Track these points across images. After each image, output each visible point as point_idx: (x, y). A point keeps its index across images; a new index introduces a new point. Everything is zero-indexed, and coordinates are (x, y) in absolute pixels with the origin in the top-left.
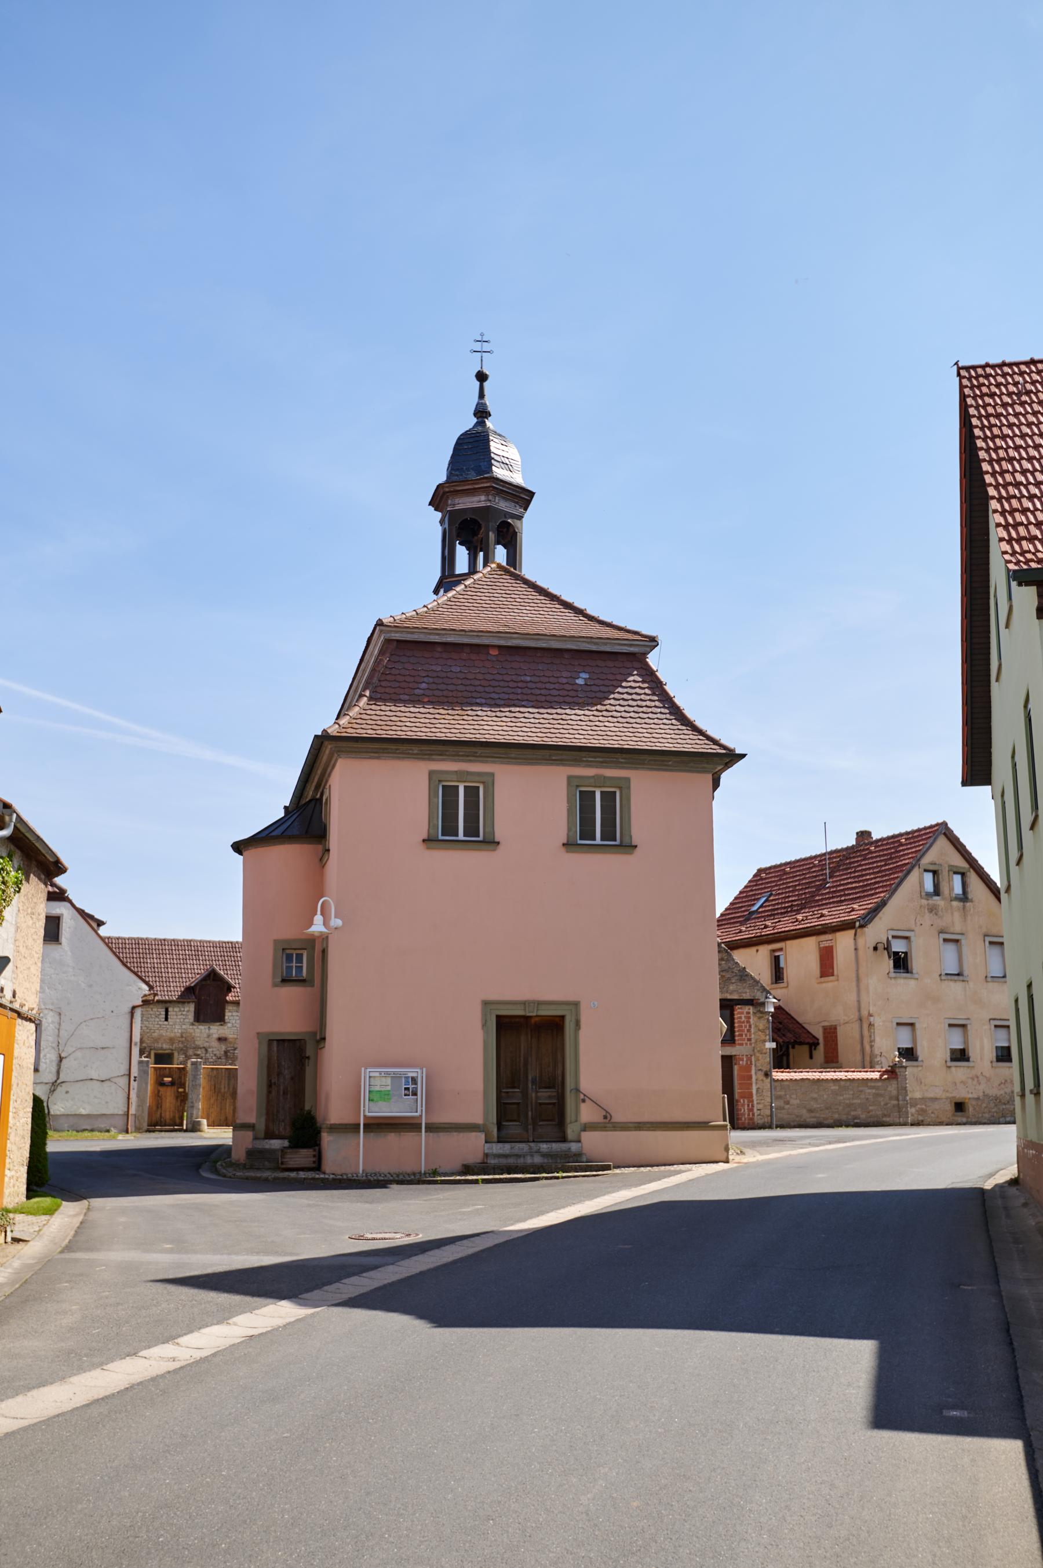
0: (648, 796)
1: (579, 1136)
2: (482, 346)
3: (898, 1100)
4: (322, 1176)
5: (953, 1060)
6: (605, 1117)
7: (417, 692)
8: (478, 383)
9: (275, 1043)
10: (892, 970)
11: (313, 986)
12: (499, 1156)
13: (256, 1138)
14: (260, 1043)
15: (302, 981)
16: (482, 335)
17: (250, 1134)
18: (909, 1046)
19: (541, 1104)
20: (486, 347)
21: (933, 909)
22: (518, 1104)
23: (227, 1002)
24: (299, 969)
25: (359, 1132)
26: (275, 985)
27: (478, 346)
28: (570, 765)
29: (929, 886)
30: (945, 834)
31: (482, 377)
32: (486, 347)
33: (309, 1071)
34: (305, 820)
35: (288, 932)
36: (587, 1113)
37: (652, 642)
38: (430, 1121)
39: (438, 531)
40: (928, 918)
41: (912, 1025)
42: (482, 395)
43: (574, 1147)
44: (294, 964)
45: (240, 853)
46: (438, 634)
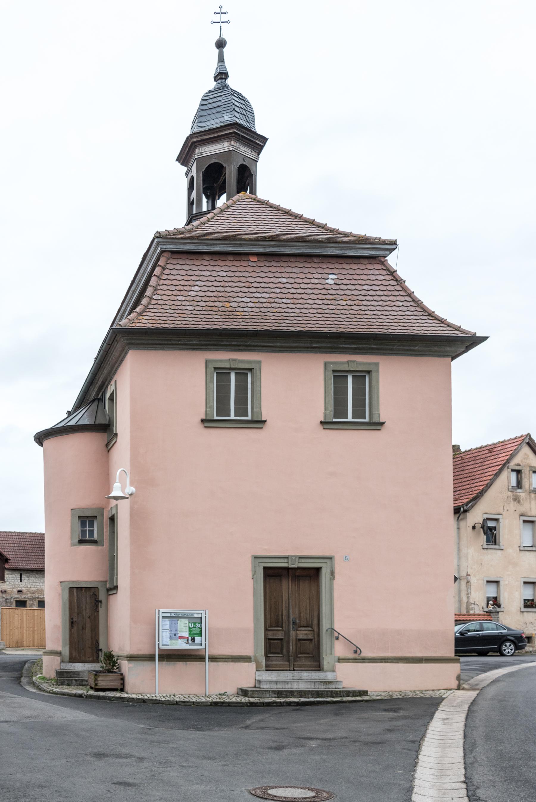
1: (334, 666)
2: (221, 17)
5: (526, 606)
6: (355, 652)
7: (192, 293)
8: (217, 51)
9: (75, 589)
10: (485, 543)
12: (271, 682)
14: (63, 590)
15: (95, 542)
16: (221, 7)
17: (58, 659)
18: (495, 596)
19: (300, 640)
20: (224, 18)
21: (516, 499)
23: (6, 569)
24: (91, 533)
25: (155, 661)
26: (73, 545)
27: (217, 18)
28: (326, 352)
29: (514, 483)
30: (528, 444)
31: (221, 44)
32: (224, 18)
33: (101, 611)
35: (86, 501)
36: (340, 649)
37: (391, 245)
38: (210, 654)
40: (513, 506)
41: (497, 582)
42: (221, 59)
43: (330, 676)
44: (87, 529)
45: (41, 444)
46: (206, 244)
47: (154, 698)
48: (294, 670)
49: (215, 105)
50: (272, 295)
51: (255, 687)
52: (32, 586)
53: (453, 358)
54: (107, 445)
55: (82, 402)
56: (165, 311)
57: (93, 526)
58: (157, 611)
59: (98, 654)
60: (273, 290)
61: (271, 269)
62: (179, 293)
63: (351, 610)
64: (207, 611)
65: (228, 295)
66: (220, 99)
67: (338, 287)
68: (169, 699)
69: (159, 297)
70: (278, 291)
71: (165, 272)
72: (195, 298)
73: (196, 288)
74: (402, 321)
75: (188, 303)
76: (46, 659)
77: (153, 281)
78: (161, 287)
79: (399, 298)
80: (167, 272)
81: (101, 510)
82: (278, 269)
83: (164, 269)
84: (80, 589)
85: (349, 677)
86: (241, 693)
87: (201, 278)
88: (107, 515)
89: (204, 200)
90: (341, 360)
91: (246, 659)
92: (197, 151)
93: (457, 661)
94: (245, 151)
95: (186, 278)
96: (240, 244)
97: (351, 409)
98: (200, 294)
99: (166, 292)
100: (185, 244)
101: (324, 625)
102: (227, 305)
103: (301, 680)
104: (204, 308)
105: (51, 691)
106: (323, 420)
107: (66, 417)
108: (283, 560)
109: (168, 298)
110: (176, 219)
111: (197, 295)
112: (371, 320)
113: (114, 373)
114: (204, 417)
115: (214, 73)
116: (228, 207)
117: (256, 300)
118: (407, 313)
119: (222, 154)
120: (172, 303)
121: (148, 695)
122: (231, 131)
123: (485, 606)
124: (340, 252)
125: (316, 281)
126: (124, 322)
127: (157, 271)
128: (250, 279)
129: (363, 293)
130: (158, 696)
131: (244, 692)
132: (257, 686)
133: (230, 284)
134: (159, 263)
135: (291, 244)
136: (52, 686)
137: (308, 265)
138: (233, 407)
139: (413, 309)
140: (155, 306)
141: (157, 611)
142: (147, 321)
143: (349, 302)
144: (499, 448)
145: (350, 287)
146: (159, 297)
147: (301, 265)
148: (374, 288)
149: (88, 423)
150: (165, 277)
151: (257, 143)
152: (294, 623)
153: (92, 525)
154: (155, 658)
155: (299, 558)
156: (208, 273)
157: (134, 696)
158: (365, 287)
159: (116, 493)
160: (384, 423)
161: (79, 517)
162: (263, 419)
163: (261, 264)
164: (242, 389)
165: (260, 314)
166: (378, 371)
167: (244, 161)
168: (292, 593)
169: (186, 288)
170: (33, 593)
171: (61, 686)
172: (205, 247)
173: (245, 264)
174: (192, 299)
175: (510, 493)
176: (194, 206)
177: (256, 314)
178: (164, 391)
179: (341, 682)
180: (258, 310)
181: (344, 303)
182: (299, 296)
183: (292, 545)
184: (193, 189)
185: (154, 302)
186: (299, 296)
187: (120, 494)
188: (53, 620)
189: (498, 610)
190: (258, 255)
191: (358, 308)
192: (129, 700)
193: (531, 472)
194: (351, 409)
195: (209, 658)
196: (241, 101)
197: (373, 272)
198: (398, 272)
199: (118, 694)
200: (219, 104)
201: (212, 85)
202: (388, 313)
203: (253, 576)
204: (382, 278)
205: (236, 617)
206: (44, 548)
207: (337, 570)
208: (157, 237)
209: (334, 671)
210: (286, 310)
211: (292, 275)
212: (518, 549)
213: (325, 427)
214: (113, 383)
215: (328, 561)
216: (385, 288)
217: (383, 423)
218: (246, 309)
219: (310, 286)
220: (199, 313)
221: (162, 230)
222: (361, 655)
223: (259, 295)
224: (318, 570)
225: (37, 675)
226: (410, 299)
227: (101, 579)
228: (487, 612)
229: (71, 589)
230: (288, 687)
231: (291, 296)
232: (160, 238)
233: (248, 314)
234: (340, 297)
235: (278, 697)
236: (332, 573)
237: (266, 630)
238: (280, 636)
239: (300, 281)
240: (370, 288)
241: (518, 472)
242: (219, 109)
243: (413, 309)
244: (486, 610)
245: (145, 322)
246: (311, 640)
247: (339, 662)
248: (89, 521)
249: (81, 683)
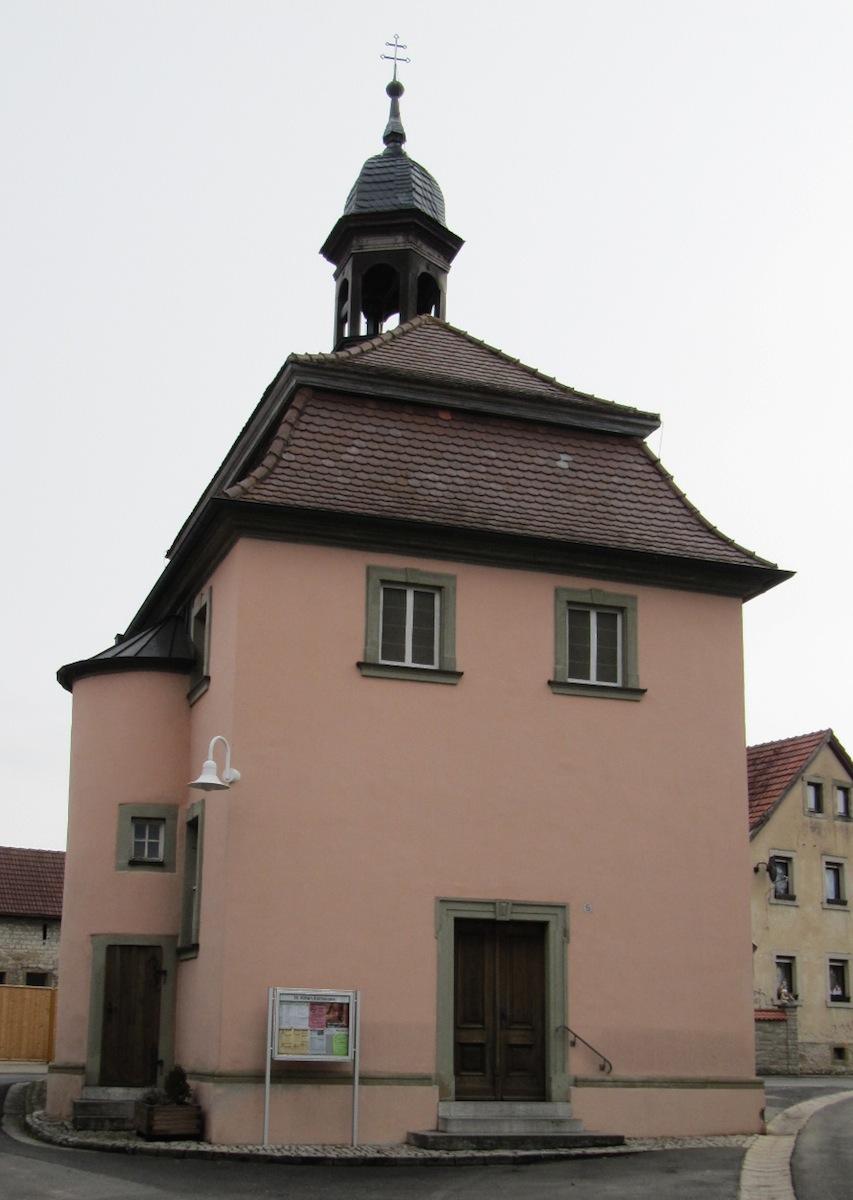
0: (659, 622)
3: (787, 1044)
4: (209, 1148)
6: (602, 1068)
7: (345, 457)
8: (389, 99)
11: (174, 871)
13: (87, 1085)
14: (95, 949)
15: (159, 865)
16: (397, 37)
17: (79, 1079)
20: (401, 53)
21: (815, 828)
22: (481, 1045)
24: (154, 848)
25: (264, 1082)
26: (119, 868)
27: (390, 51)
29: (811, 804)
31: (395, 90)
32: (401, 53)
33: (165, 989)
34: (169, 634)
35: (148, 791)
36: (578, 1063)
37: (651, 421)
39: (331, 289)
42: (395, 112)
44: (146, 840)
46: (372, 384)
47: (262, 1152)
48: (502, 1100)
49: (385, 178)
50: (474, 475)
51: (437, 1130)
52: (17, 947)
53: (744, 601)
54: (189, 696)
55: (146, 619)
56: (302, 480)
57: (160, 834)
58: (271, 990)
59: (156, 1070)
60: (476, 468)
61: (472, 435)
62: (325, 455)
63: (594, 995)
64: (359, 993)
65: (404, 466)
66: (392, 170)
67: (573, 474)
68: (289, 1154)
69: (293, 457)
70: (483, 469)
71: (302, 418)
72: (351, 466)
73: (354, 450)
74: (670, 535)
75: (340, 472)
76: (54, 1081)
77: (283, 430)
78: (297, 442)
79: (664, 501)
80: (305, 418)
81: (173, 809)
82: (484, 436)
83: (301, 413)
84: (127, 949)
85: (589, 1111)
86: (413, 1141)
87: (361, 435)
88: (183, 819)
89: (363, 321)
90: (581, 586)
91: (423, 1080)
92: (354, 242)
93: (759, 1085)
94: (428, 253)
95: (337, 432)
96: (424, 391)
97: (595, 664)
98: (359, 459)
99: (304, 451)
100: (336, 378)
101: (552, 1021)
102: (402, 481)
103: (511, 1118)
104: (366, 483)
105: (65, 1142)
106: (552, 679)
107: (113, 644)
108: (486, 908)
109: (306, 460)
110: (319, 341)
111: (344, 463)
112: (624, 530)
113: (209, 575)
114: (362, 660)
115: (384, 131)
116: (404, 333)
117: (449, 480)
118: (676, 524)
119: (391, 243)
120: (313, 468)
121: (250, 1147)
122: (410, 220)
123: (775, 997)
124: (577, 423)
125: (542, 462)
126: (232, 492)
127: (291, 415)
128: (440, 447)
129: (612, 487)
130: (268, 1146)
131: (420, 1141)
132: (440, 1128)
133: (409, 450)
134: (293, 404)
135: (505, 400)
136: (65, 1131)
137: (529, 436)
138: (408, 645)
139: (686, 520)
140: (286, 471)
141: (271, 990)
142: (271, 493)
143: (591, 499)
144: (788, 749)
145: (592, 476)
146: (293, 457)
147: (519, 434)
148: (627, 481)
149: (158, 655)
150: (303, 426)
151: (449, 245)
152: (503, 1016)
153: (155, 834)
154: (264, 1077)
155: (514, 904)
156: (374, 429)
157: (224, 1149)
158: (616, 479)
159: (208, 777)
160: (645, 691)
161: (133, 818)
162: (458, 669)
163: (456, 425)
164: (424, 619)
165: (455, 501)
166: (635, 609)
167: (428, 268)
168: (501, 965)
169: (336, 448)
170: (19, 959)
171: (84, 1132)
172: (370, 388)
173: (432, 421)
174: (345, 465)
175: (807, 819)
176: (347, 326)
177: (448, 501)
178: (291, 611)
179: (580, 1120)
180: (452, 495)
181: (585, 499)
182: (516, 481)
183: (504, 882)
184: (347, 299)
185: (282, 464)
186: (516, 481)
187: (215, 780)
188: (75, 1001)
189: (796, 1003)
190: (454, 411)
191: (604, 509)
192: (215, 1156)
193: (835, 788)
194: (595, 664)
195: (360, 1078)
196: (424, 179)
197: (627, 459)
198: (661, 462)
199: (193, 1146)
200: (392, 177)
201: (380, 148)
202: (649, 522)
203: (437, 933)
204: (640, 468)
205: (410, 1004)
206: (63, 869)
207: (573, 927)
208: (292, 362)
209: (568, 1101)
210: (496, 500)
211: (504, 448)
212: (820, 906)
213: (556, 690)
214: (205, 590)
215: (558, 911)
216: (643, 484)
217: (644, 691)
218: (433, 492)
219: (532, 467)
220: (357, 489)
221: (301, 351)
222: (612, 1073)
223: (454, 473)
224: (542, 927)
225: (33, 1110)
226: (681, 505)
227: (169, 932)
228: (779, 1007)
229: (111, 949)
230: (492, 1131)
231: (504, 480)
232: (296, 365)
233: (436, 499)
234: (577, 490)
235: (479, 1149)
236: (566, 933)
237: (457, 1028)
238: (477, 1038)
239: (518, 458)
240: (622, 480)
241: (818, 787)
242: (391, 186)
243: (686, 520)
244: (778, 1002)
245: (268, 495)
246: (530, 1047)
247: (576, 1086)
248: (151, 827)
249: (118, 1125)
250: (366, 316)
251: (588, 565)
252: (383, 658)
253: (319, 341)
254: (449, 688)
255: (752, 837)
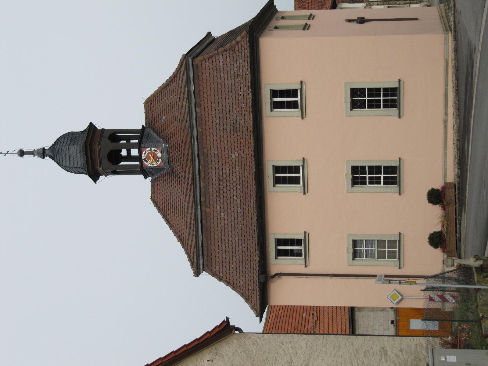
8: (25, 156)
31: (22, 153)
42: (32, 153)
119: (94, 152)
250: (121, 163)
251: (256, 66)
252: (396, 259)
253: (141, 185)
254: (404, 236)
255: (423, 6)
